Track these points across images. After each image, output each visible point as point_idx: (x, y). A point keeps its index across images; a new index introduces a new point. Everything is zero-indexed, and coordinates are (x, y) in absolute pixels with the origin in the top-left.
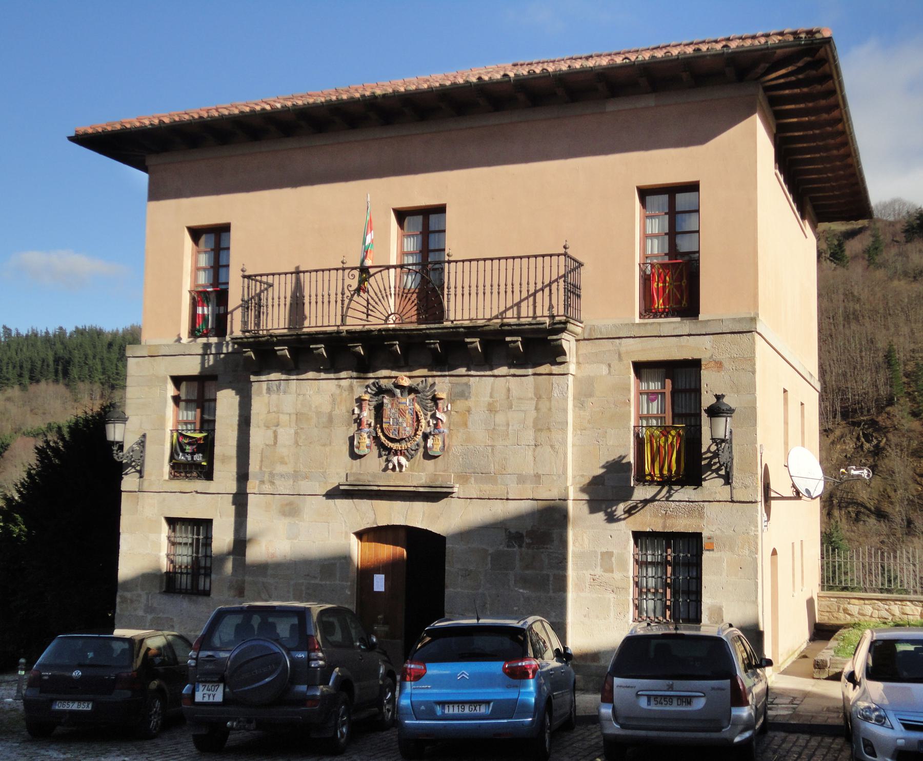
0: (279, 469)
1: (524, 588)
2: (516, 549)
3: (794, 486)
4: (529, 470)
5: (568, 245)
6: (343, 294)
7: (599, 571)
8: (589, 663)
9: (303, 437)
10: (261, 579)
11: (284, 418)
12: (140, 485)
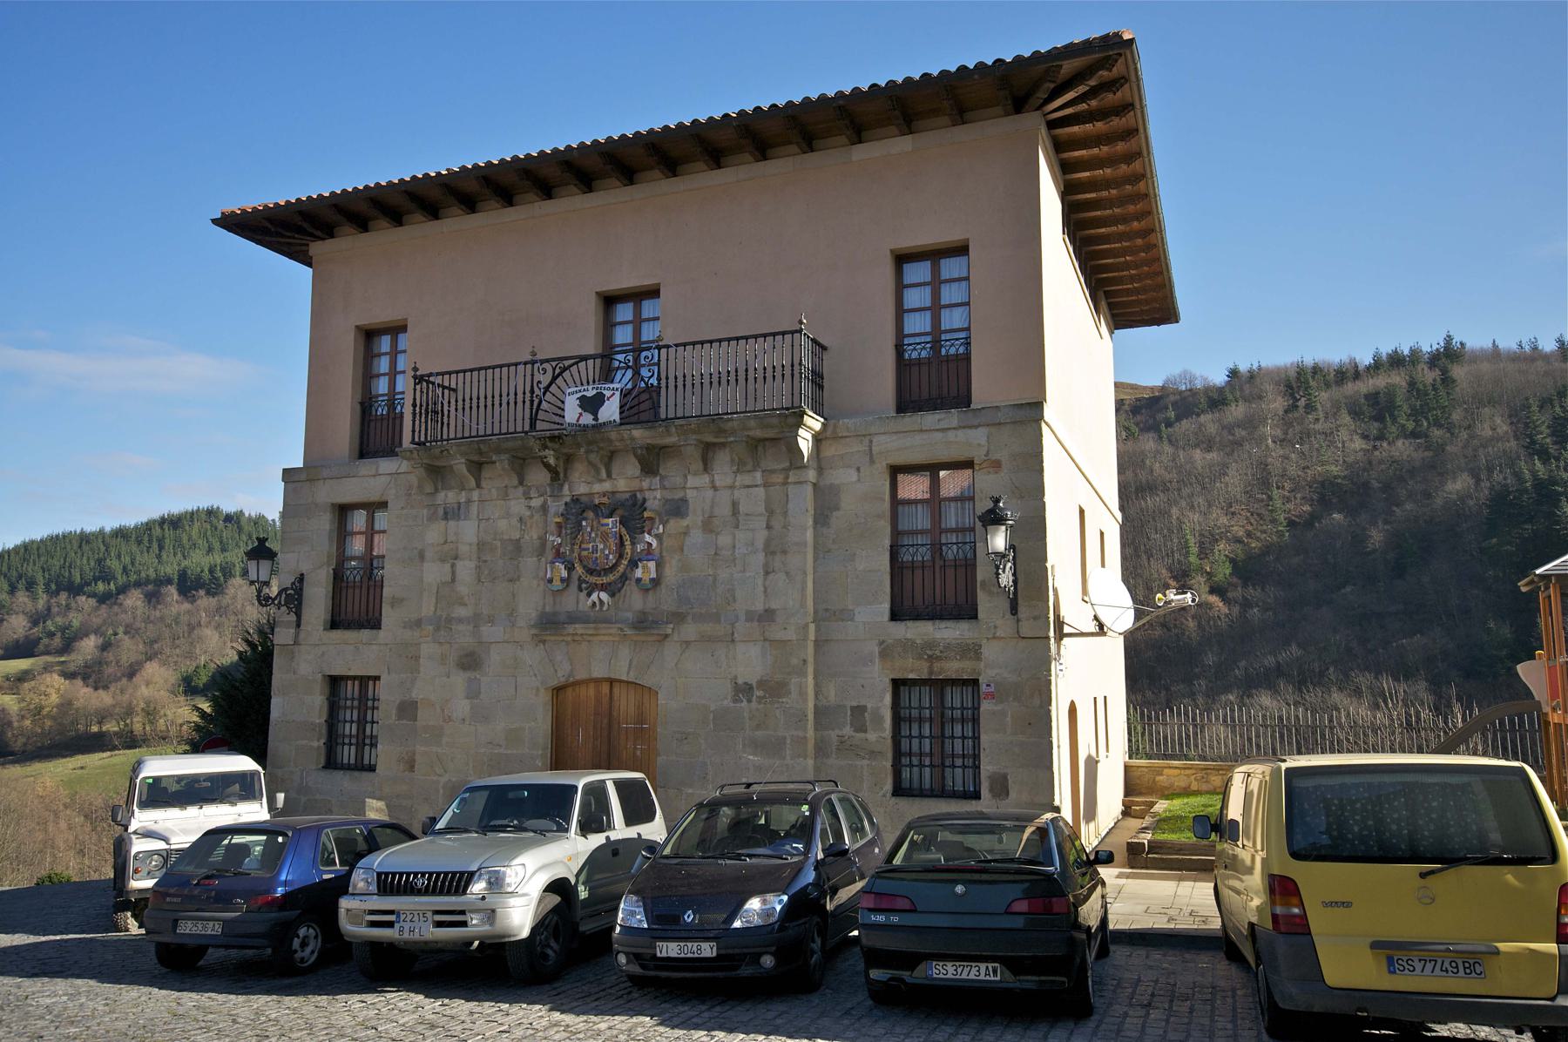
1: (755, 754)
3: (1096, 618)
6: (532, 392)
7: (848, 731)
10: (434, 749)
11: (463, 549)
12: (297, 635)
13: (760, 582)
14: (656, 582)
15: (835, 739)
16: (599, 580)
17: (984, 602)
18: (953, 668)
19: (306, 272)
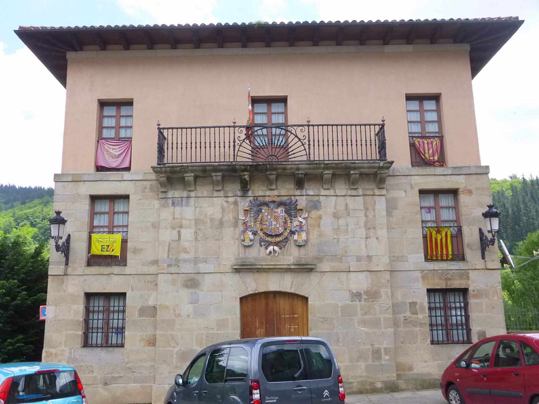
0: (183, 256)
2: (358, 303)
4: (364, 253)
5: (385, 119)
6: (234, 142)
7: (408, 314)
8: (407, 372)
9: (201, 235)
11: (185, 222)
12: (66, 270)
13: (363, 243)
14: (306, 241)
15: (402, 319)
17: (468, 253)
18: (457, 284)
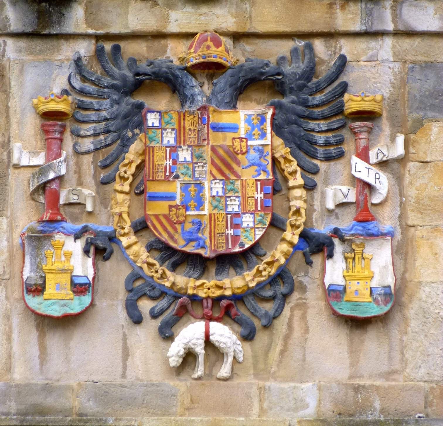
16: (207, 286)
19: (327, 207)
